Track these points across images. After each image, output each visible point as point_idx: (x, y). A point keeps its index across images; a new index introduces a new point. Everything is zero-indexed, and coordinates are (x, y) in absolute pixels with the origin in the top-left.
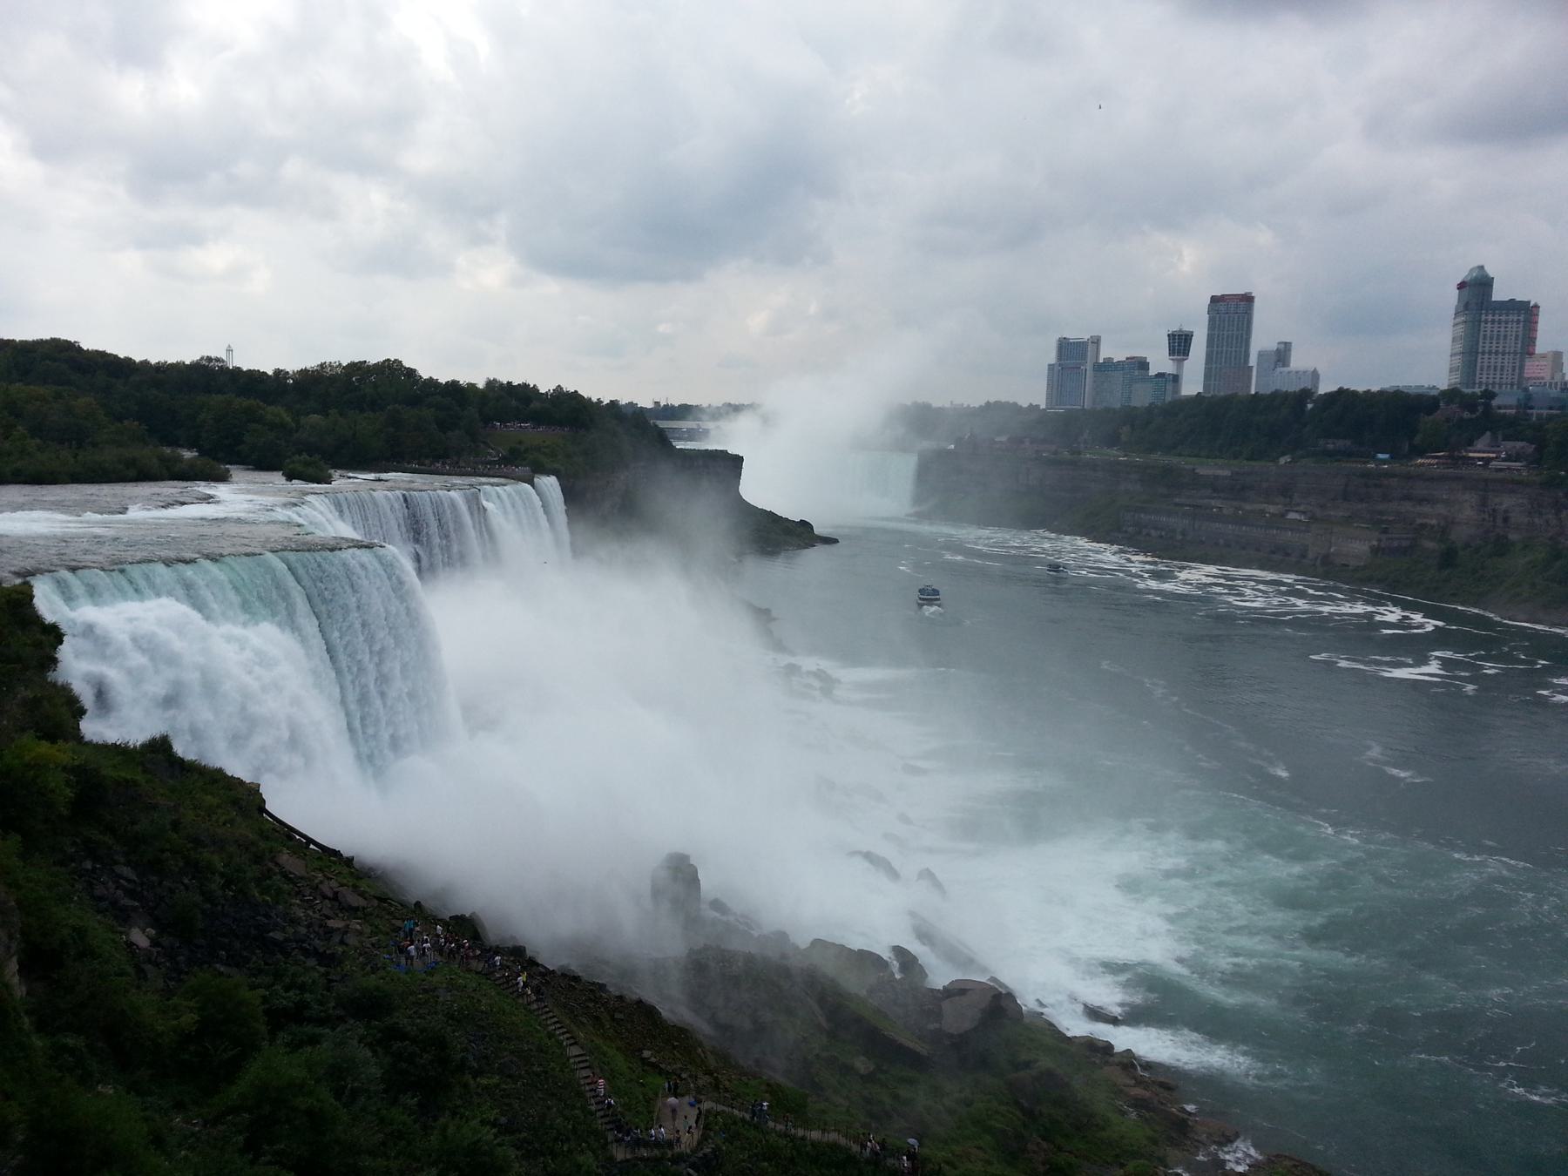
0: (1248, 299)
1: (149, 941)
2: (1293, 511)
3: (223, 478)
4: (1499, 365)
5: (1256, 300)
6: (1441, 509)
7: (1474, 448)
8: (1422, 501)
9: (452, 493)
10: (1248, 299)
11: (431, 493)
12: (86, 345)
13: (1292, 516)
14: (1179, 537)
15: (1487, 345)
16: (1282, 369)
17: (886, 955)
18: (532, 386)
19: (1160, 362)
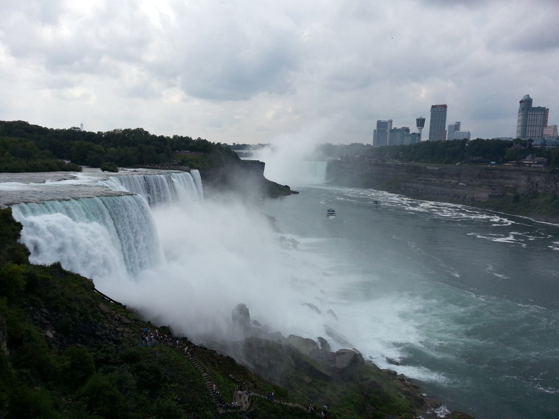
0: (445, 107)
1: (53, 335)
2: (461, 182)
3: (79, 170)
4: (534, 130)
5: (448, 107)
6: (514, 181)
7: (526, 160)
8: (507, 178)
9: (161, 176)
10: (445, 107)
11: (154, 175)
13: (461, 184)
14: (420, 191)
15: (530, 123)
16: (457, 132)
18: (189, 137)
19: (414, 129)
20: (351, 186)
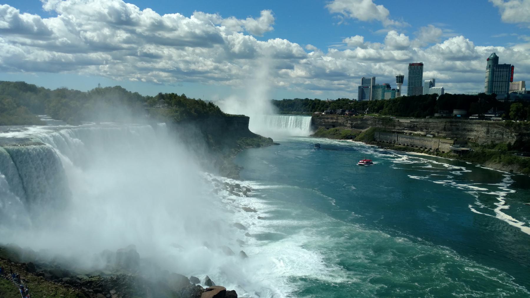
2: (428, 134)
4: (501, 85)
13: (428, 135)
15: (497, 79)
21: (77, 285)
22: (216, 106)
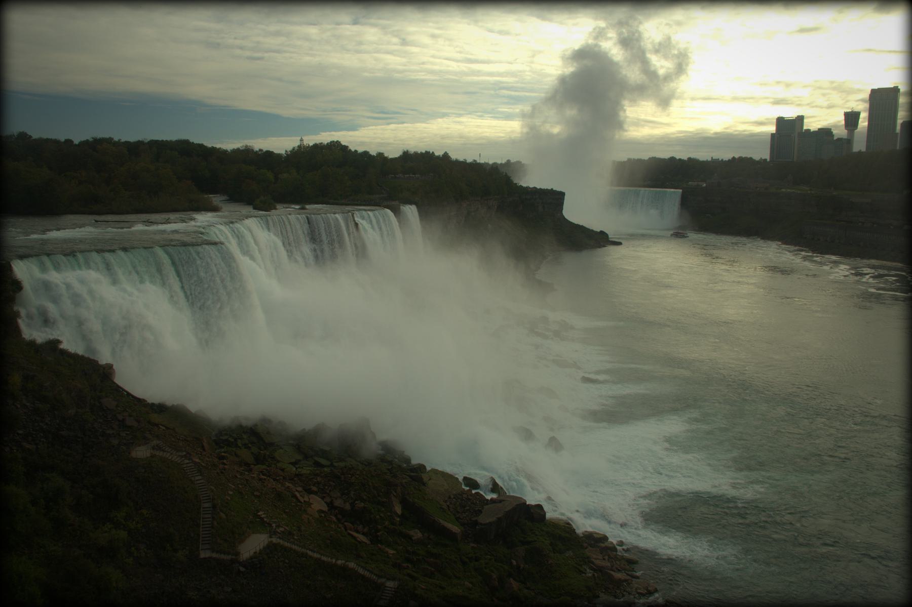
9: (337, 215)
11: (323, 215)
12: (195, 142)
17: (461, 479)
18: (431, 153)
20: (901, 293)
21: (278, 478)
22: (504, 174)
